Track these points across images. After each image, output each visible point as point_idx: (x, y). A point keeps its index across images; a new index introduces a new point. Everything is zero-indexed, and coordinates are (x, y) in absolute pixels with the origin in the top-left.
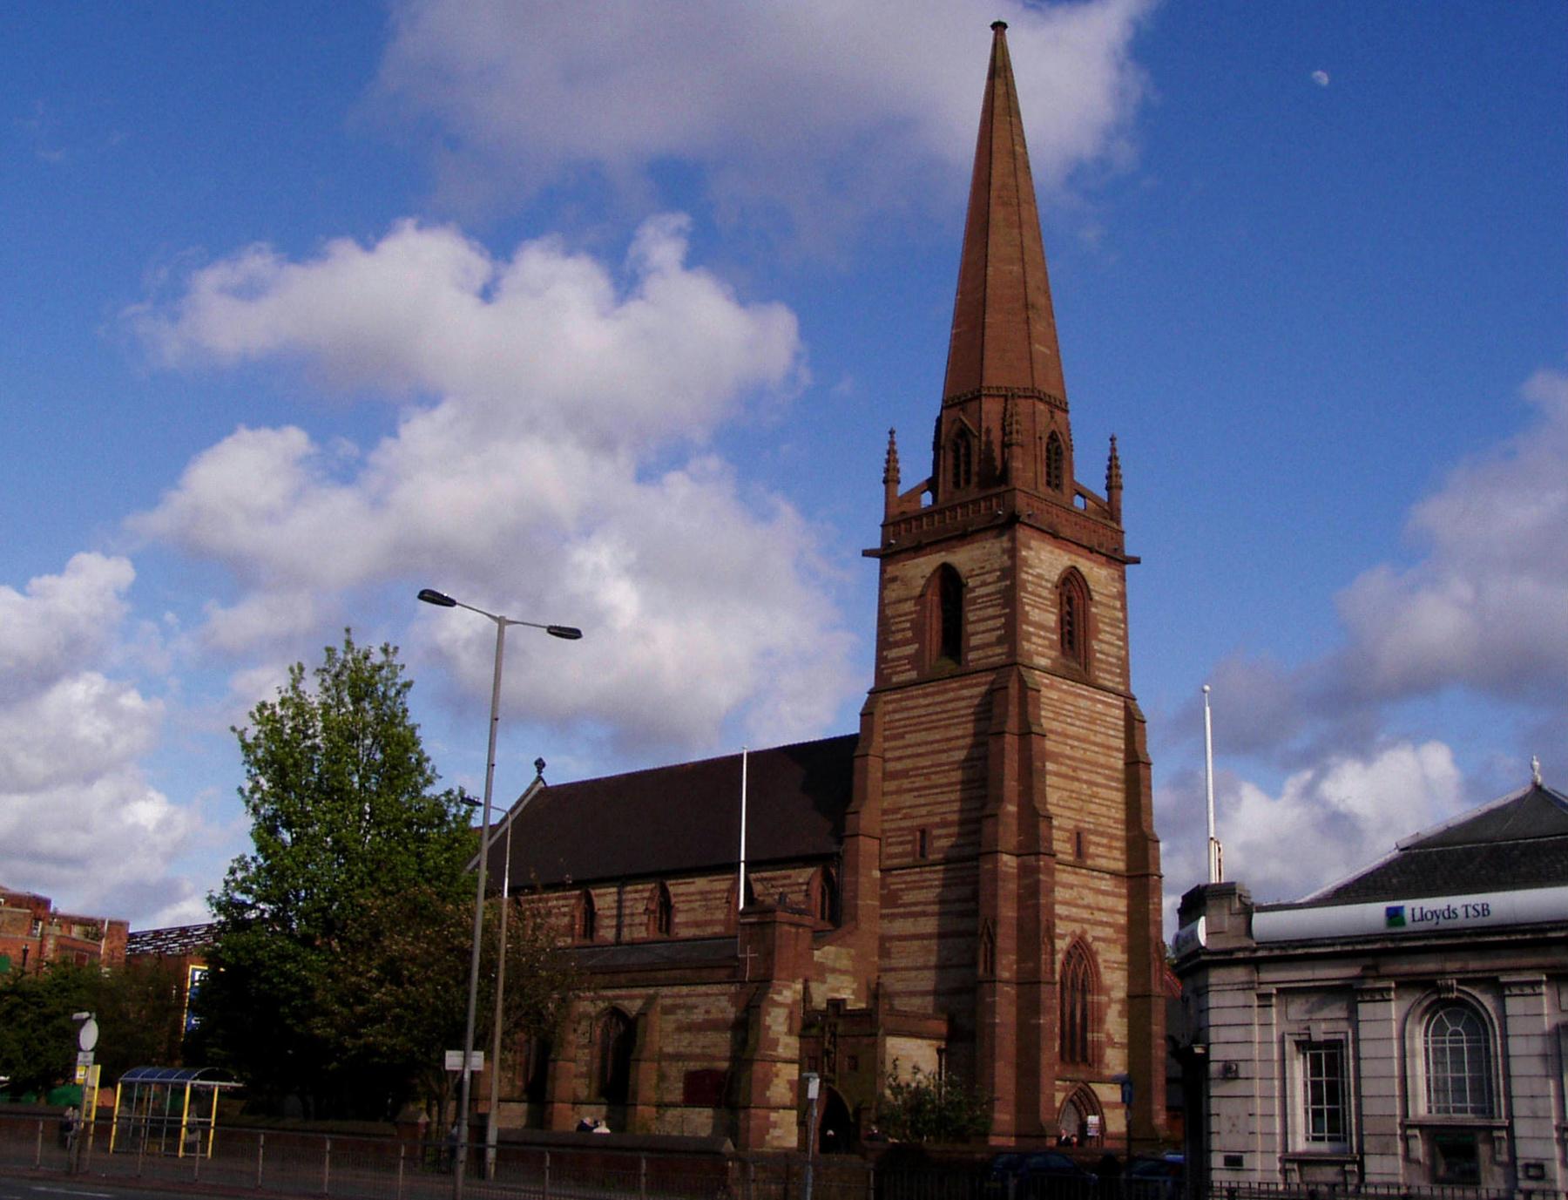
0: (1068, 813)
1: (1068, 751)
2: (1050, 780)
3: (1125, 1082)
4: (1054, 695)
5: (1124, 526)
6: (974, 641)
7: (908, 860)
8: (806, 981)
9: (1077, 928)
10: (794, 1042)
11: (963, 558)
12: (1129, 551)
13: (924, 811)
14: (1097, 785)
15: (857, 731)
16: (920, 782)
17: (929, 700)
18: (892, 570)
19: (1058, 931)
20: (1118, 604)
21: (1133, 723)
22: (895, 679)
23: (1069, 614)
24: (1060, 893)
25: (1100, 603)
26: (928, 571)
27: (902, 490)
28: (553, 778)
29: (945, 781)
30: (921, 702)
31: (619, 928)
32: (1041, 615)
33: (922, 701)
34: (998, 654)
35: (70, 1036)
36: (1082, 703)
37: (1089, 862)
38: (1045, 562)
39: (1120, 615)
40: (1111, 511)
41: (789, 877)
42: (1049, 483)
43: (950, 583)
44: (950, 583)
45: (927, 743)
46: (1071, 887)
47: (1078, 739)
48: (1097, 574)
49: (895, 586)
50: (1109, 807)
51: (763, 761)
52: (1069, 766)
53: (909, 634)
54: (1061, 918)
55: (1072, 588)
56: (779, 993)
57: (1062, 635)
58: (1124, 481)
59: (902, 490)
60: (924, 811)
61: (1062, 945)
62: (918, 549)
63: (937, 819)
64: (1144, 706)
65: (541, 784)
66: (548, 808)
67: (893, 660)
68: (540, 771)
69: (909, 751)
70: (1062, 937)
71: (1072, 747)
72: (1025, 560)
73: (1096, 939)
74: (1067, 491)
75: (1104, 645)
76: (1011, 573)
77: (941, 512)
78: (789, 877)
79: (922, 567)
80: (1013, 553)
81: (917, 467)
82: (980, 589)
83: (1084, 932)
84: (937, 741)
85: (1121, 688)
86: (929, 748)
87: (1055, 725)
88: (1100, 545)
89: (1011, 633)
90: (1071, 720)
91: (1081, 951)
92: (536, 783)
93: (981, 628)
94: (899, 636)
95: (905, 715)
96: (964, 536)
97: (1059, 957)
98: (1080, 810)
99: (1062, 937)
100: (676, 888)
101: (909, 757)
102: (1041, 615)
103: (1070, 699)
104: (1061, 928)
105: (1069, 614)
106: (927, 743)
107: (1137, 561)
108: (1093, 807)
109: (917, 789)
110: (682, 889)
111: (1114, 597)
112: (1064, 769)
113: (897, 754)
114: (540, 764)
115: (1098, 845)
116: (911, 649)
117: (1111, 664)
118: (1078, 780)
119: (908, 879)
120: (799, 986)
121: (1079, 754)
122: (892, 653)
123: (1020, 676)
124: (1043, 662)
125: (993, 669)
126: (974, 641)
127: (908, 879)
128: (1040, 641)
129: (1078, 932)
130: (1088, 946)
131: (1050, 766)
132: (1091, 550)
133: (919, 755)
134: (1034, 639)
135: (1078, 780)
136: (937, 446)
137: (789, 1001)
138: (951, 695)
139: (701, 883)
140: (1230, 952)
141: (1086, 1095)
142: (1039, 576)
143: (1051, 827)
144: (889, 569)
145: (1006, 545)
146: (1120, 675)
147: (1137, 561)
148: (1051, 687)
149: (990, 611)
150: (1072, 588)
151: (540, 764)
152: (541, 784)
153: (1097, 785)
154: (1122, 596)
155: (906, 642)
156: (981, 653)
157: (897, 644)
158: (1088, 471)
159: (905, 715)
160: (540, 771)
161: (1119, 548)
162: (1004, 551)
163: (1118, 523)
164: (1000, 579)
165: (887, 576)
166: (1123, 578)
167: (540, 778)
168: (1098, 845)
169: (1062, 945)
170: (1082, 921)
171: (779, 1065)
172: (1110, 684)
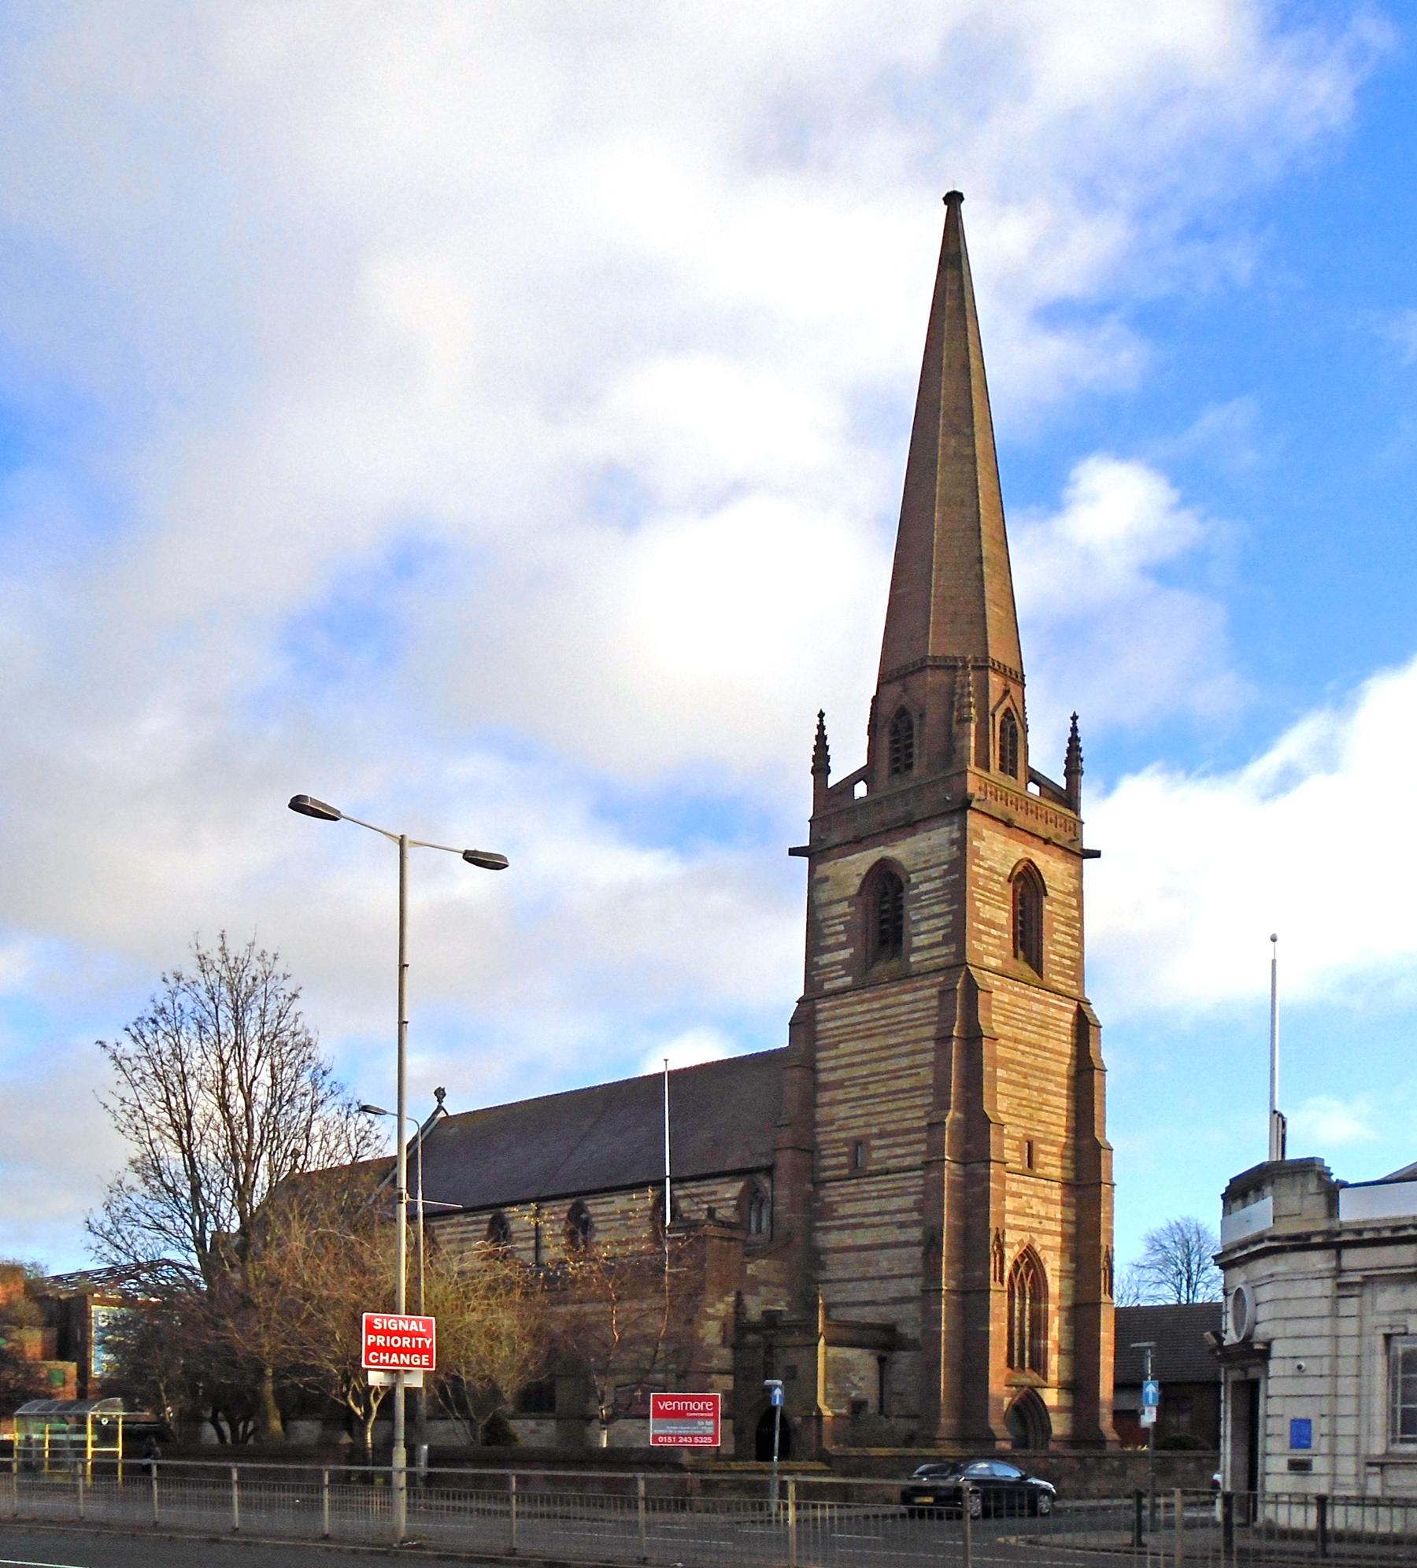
0: (1018, 1121)
1: (1019, 1057)
2: (1001, 1087)
3: (1065, 1387)
4: (1006, 998)
5: (1084, 815)
6: (917, 941)
7: (846, 1172)
8: (739, 1294)
9: (1025, 1237)
10: (726, 1352)
11: (900, 851)
12: (1088, 844)
13: (861, 1122)
14: (1048, 1092)
15: (787, 1044)
16: (856, 1092)
17: (865, 1007)
18: (824, 869)
19: (1007, 1239)
20: (1074, 902)
21: (1084, 1026)
22: (827, 986)
23: (1022, 913)
24: (1010, 1203)
25: (1054, 900)
26: (864, 869)
27: (833, 780)
28: (454, 1106)
29: (883, 1090)
30: (857, 1010)
31: (538, 1248)
32: (991, 914)
33: (859, 1008)
34: (942, 955)
35: (1000, 1544)
36: (1036, 1007)
37: (1038, 1171)
38: (995, 852)
39: (1076, 914)
40: (1069, 798)
41: (714, 1193)
42: (1002, 768)
43: (886, 884)
44: (886, 884)
45: (865, 1052)
46: (1019, 1195)
47: (1032, 1046)
48: (1052, 867)
49: (827, 886)
50: (1054, 1121)
51: (679, 1077)
52: (1018, 1073)
53: (843, 938)
54: (1010, 1228)
55: (1028, 885)
56: (712, 1306)
57: (1014, 935)
58: (1084, 765)
59: (833, 780)
60: (861, 1122)
61: (1011, 1254)
62: (858, 843)
63: (875, 1130)
64: (1100, 1011)
65: (442, 1114)
66: (447, 1142)
67: (826, 966)
68: (440, 1101)
69: (844, 1061)
70: (1012, 1245)
71: (1023, 1053)
72: (977, 854)
73: (1044, 1247)
74: (1021, 773)
75: (1053, 950)
76: (958, 866)
77: (878, 803)
78: (714, 1193)
79: (856, 865)
80: (961, 843)
81: (850, 755)
82: (924, 886)
83: (1032, 1240)
84: (872, 1050)
85: (1076, 991)
86: (865, 1057)
87: (1006, 1030)
88: (1057, 836)
89: (957, 934)
90: (1020, 1025)
91: (1030, 1259)
92: (436, 1112)
93: (924, 934)
94: (831, 941)
95: (839, 1023)
96: (910, 826)
97: (1008, 1265)
98: (1031, 1118)
99: (1012, 1245)
100: (596, 1208)
101: (842, 1067)
102: (991, 914)
103: (1023, 1003)
104: (1010, 1237)
105: (1022, 913)
106: (865, 1052)
107: (1096, 854)
108: (1043, 1116)
109: (853, 1100)
110: (602, 1209)
111: (1069, 894)
112: (1014, 1076)
113: (832, 1063)
114: (440, 1094)
115: (1047, 1153)
116: (844, 954)
117: (1063, 965)
118: (1029, 1087)
119: (843, 1191)
120: (731, 1299)
121: (1029, 1060)
122: (826, 958)
123: (969, 975)
124: (993, 962)
125: (938, 970)
126: (917, 941)
127: (843, 1191)
128: (991, 940)
129: (1026, 1241)
130: (1035, 1254)
131: (1000, 1073)
132: (1047, 841)
133: (852, 1065)
134: (985, 938)
135: (1029, 1087)
136: (872, 730)
137: (722, 1313)
138: (890, 1001)
139: (620, 1202)
140: (1309, 1235)
141: (1033, 1401)
142: (991, 869)
143: (1001, 1135)
144: (820, 868)
145: (956, 835)
146: (1073, 978)
147: (1096, 854)
148: (1001, 989)
149: (937, 909)
150: (1028, 885)
151: (440, 1094)
152: (442, 1114)
153: (1048, 1092)
154: (1079, 893)
155: (842, 946)
156: (926, 955)
157: (829, 949)
158: (1045, 754)
159: (839, 1023)
160: (440, 1101)
161: (1077, 837)
162: (953, 842)
163: (1077, 811)
164: (947, 873)
165: (816, 876)
166: (1079, 875)
167: (440, 1108)
168: (1047, 1153)
169: (1011, 1254)
170: (1030, 1229)
171: (714, 1377)
172: (1062, 987)
